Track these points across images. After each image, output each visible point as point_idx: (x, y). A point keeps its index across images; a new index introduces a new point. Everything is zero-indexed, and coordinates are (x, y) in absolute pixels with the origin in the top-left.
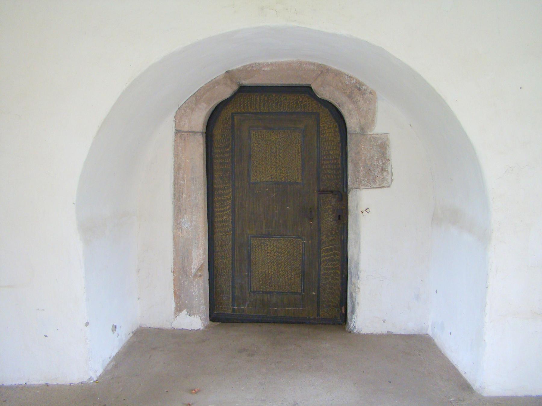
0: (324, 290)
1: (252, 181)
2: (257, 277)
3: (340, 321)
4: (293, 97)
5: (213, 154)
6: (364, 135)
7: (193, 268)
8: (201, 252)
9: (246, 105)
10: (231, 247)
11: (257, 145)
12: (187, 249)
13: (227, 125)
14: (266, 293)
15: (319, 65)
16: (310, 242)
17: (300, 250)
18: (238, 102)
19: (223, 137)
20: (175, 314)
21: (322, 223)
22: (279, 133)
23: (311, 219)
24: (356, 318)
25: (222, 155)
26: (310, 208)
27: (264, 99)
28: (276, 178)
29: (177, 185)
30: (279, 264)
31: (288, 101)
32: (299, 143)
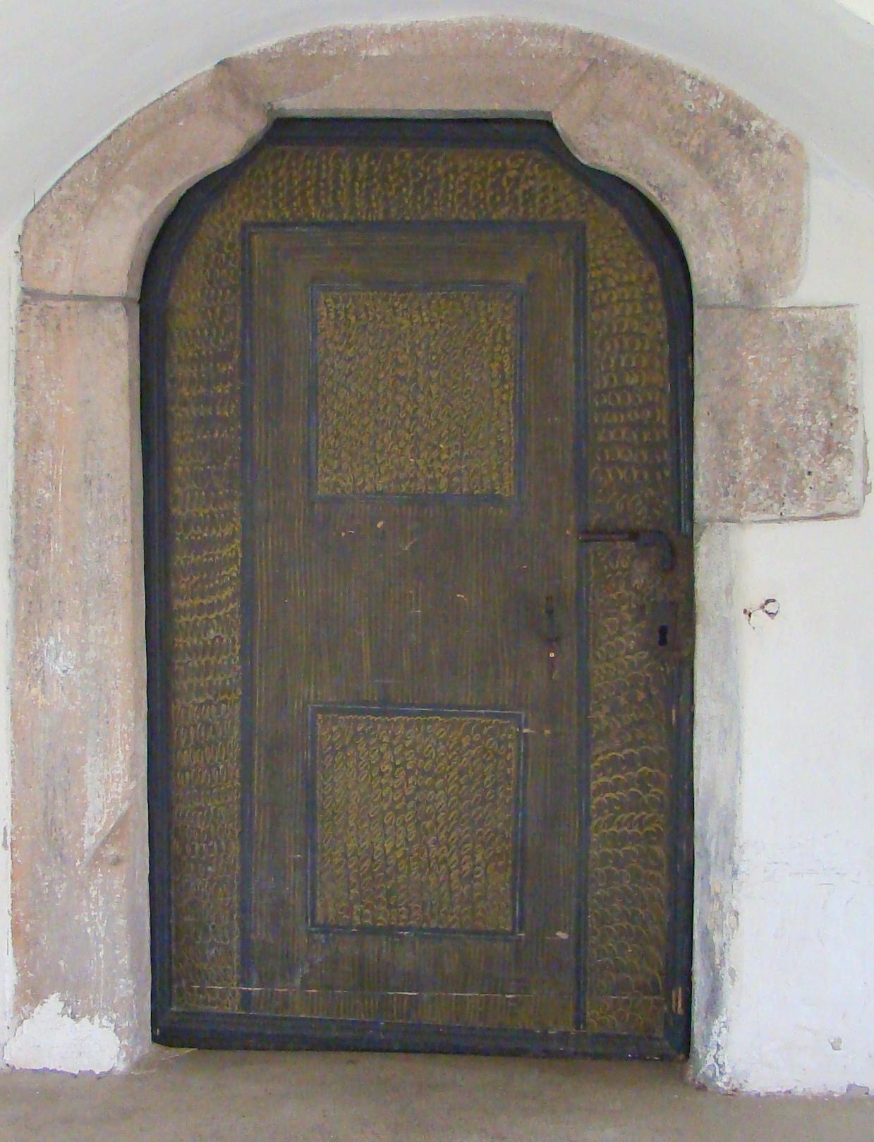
1: (322, 491)
5: (169, 386)
6: (758, 310)
8: (120, 767)
14: (374, 931)
20: (17, 1009)
21: (596, 658)
23: (552, 641)
24: (724, 1030)
25: (202, 390)
26: (549, 598)
27: (370, 168)
29: (28, 505)
30: (427, 817)
32: (505, 343)
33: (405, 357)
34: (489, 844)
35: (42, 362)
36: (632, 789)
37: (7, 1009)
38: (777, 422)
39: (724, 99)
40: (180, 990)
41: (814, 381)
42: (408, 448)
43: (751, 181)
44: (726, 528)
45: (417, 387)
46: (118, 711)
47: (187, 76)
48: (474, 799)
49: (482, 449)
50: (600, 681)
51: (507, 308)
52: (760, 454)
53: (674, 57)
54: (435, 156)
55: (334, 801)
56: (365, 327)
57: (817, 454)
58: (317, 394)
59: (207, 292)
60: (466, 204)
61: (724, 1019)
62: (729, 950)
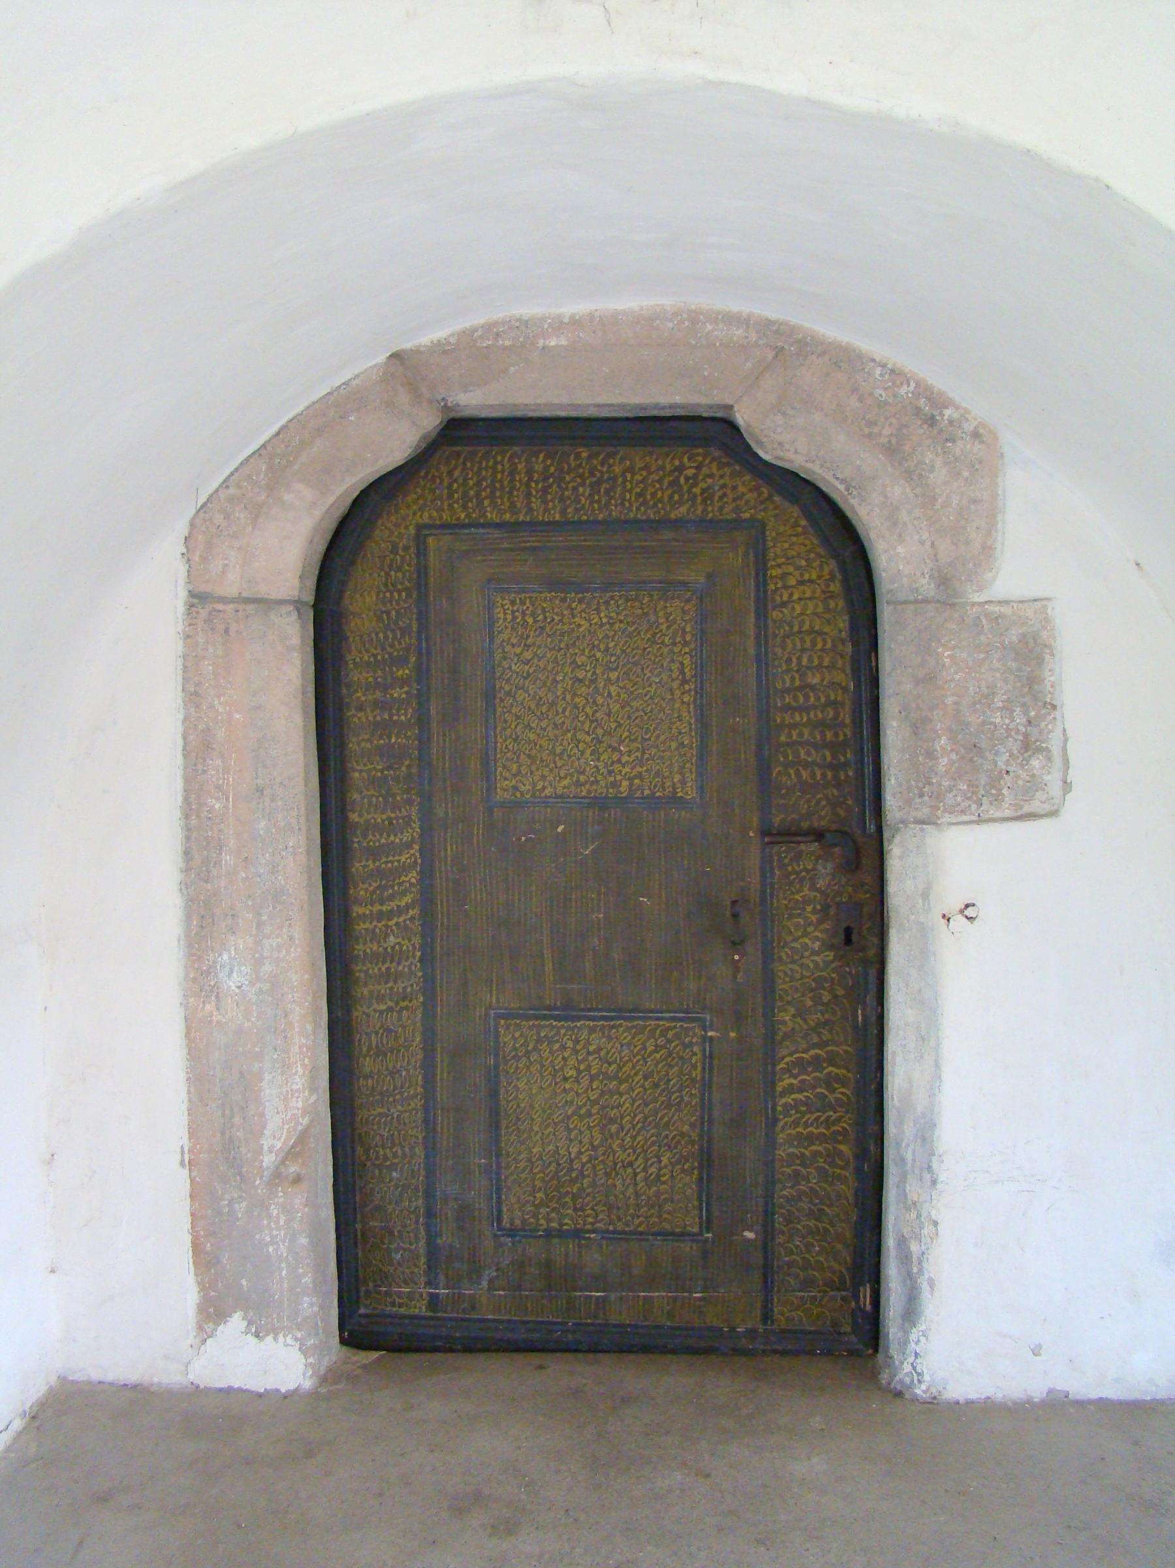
0: (789, 1222)
1: (500, 796)
2: (523, 1176)
3: (853, 1338)
4: (660, 462)
5: (344, 691)
6: (953, 605)
7: (265, 1148)
8: (299, 1082)
9: (472, 493)
10: (420, 1056)
11: (518, 650)
12: (241, 1073)
13: (400, 575)
14: (562, 1234)
15: (766, 325)
16: (733, 1035)
17: (694, 1066)
18: (442, 481)
19: (383, 621)
20: (200, 1328)
21: (780, 959)
22: (607, 603)
23: (736, 944)
24: (923, 1339)
25: (378, 694)
26: (734, 903)
27: (546, 468)
28: (597, 782)
29: (198, 816)
30: (612, 1121)
31: (638, 477)
32: (686, 644)
33: (584, 659)
34: (676, 1148)
35: (210, 668)
36: (818, 1090)
37: (190, 1327)
38: (974, 719)
39: (915, 387)
40: (368, 1293)
41: (1012, 677)
42: (589, 752)
43: (944, 471)
44: (922, 830)
45: (596, 689)
46: (296, 1025)
47: (358, 368)
48: (659, 1103)
49: (663, 751)
50: (784, 983)
51: (686, 608)
52: (957, 754)
53: (865, 345)
54: (612, 455)
55: (518, 1106)
56: (543, 628)
57: (1015, 752)
58: (494, 698)
59: (381, 596)
60: (645, 503)
61: (923, 1327)
62: (928, 1259)
